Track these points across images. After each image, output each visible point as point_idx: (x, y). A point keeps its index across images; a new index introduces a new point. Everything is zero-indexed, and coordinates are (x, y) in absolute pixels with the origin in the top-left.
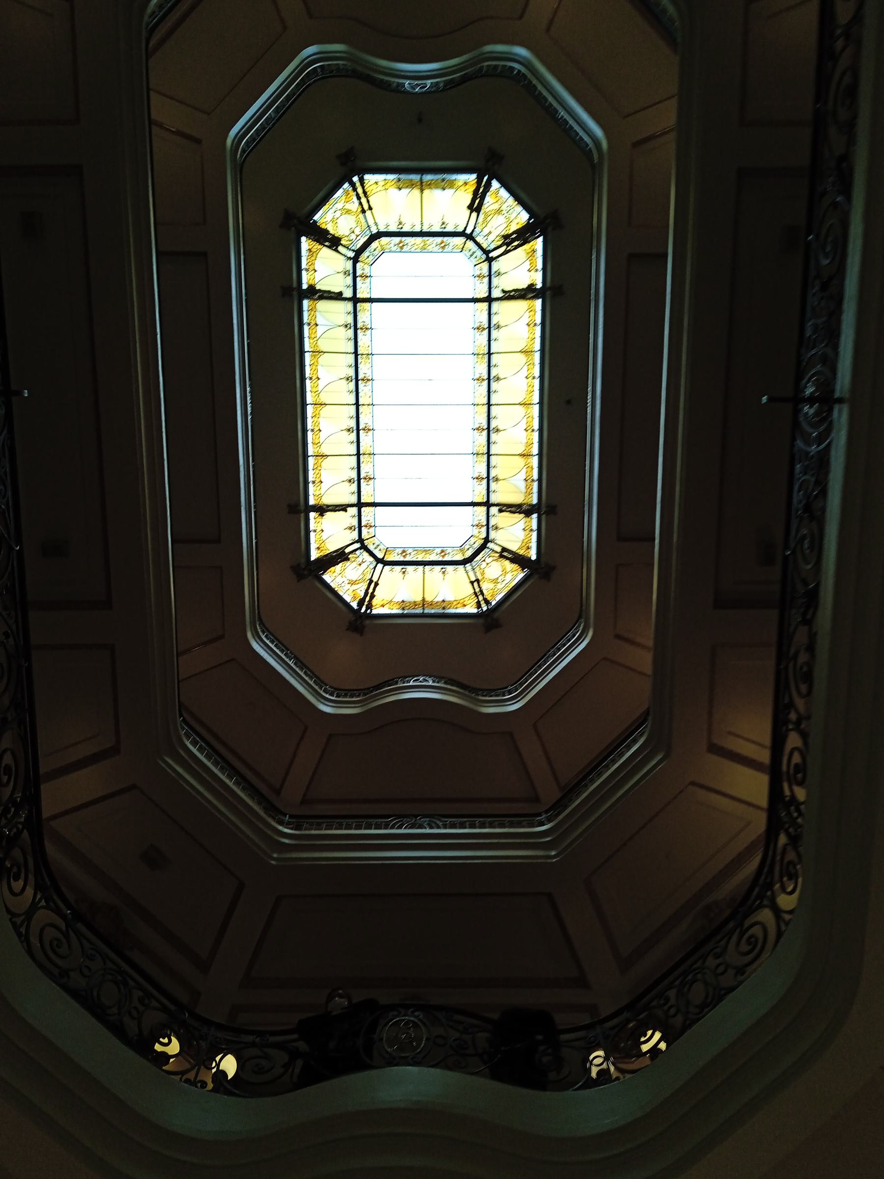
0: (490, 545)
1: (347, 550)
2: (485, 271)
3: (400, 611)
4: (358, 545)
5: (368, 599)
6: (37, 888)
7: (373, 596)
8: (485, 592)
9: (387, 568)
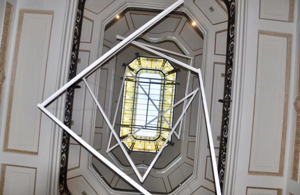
0: (136, 72)
1: (168, 74)
2: (132, 131)
3: (158, 59)
4: (166, 75)
5: (132, 147)
6: (64, 188)
7: (163, 63)
8: (138, 62)
9: (159, 69)
